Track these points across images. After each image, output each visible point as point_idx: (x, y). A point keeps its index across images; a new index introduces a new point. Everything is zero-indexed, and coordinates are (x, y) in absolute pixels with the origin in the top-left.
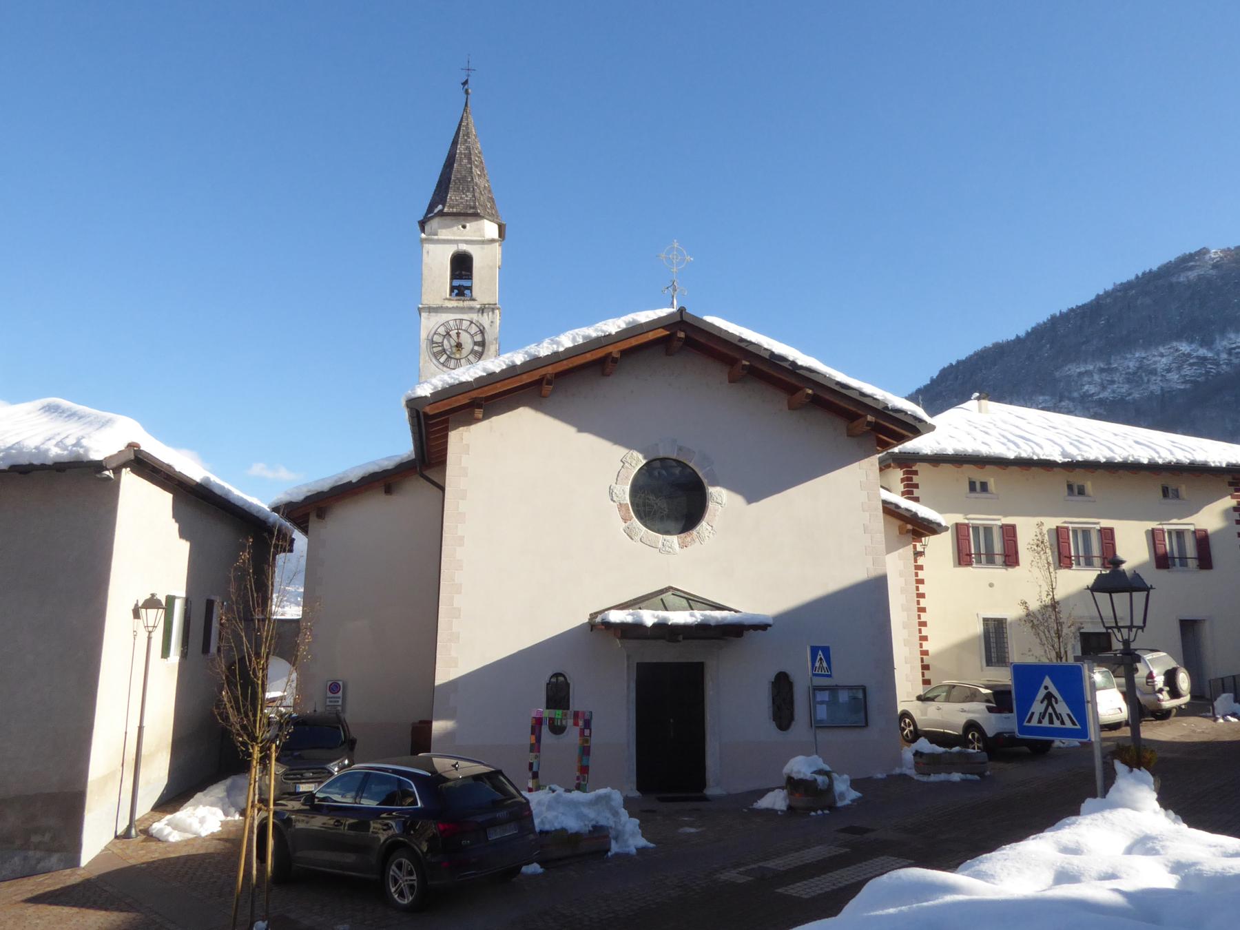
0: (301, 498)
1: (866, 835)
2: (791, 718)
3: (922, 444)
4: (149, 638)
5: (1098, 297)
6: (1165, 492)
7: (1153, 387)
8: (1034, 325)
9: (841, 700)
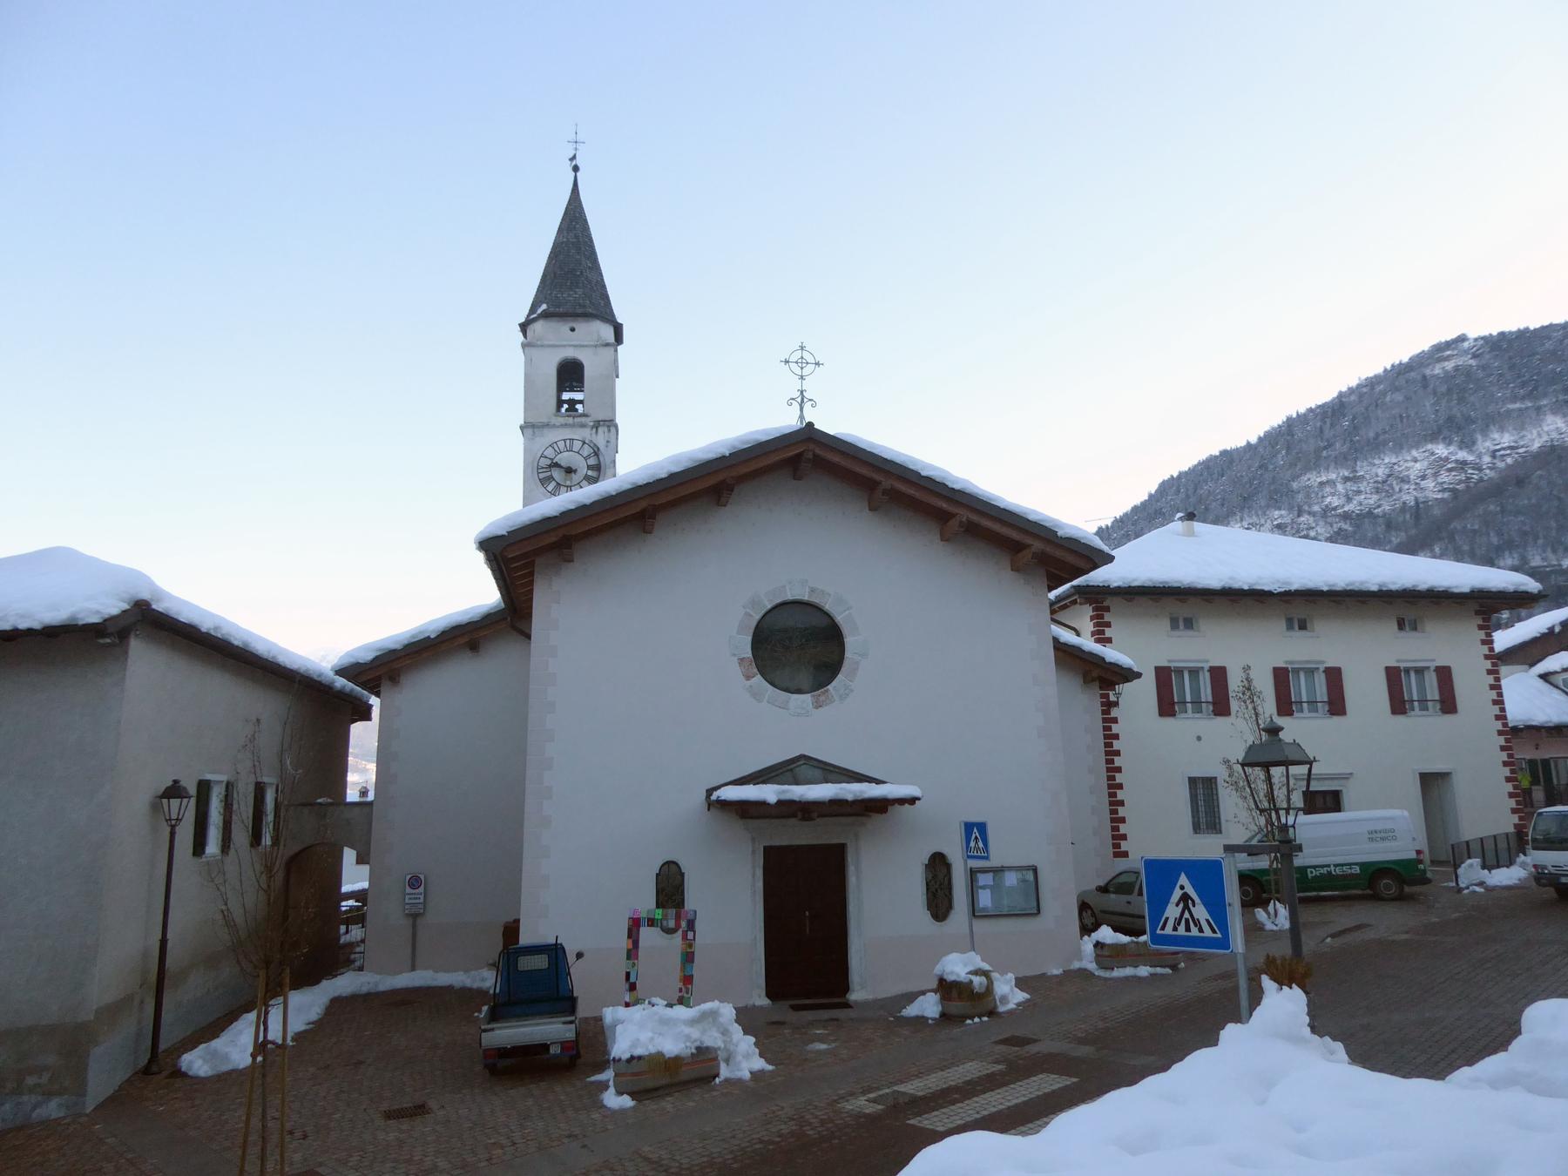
0: (369, 656)
1: (1027, 1048)
2: (950, 907)
3: (1100, 576)
4: (172, 834)
5: (1341, 395)
6: (1401, 625)
7: (1405, 497)
8: (1267, 428)
9: (1008, 883)
